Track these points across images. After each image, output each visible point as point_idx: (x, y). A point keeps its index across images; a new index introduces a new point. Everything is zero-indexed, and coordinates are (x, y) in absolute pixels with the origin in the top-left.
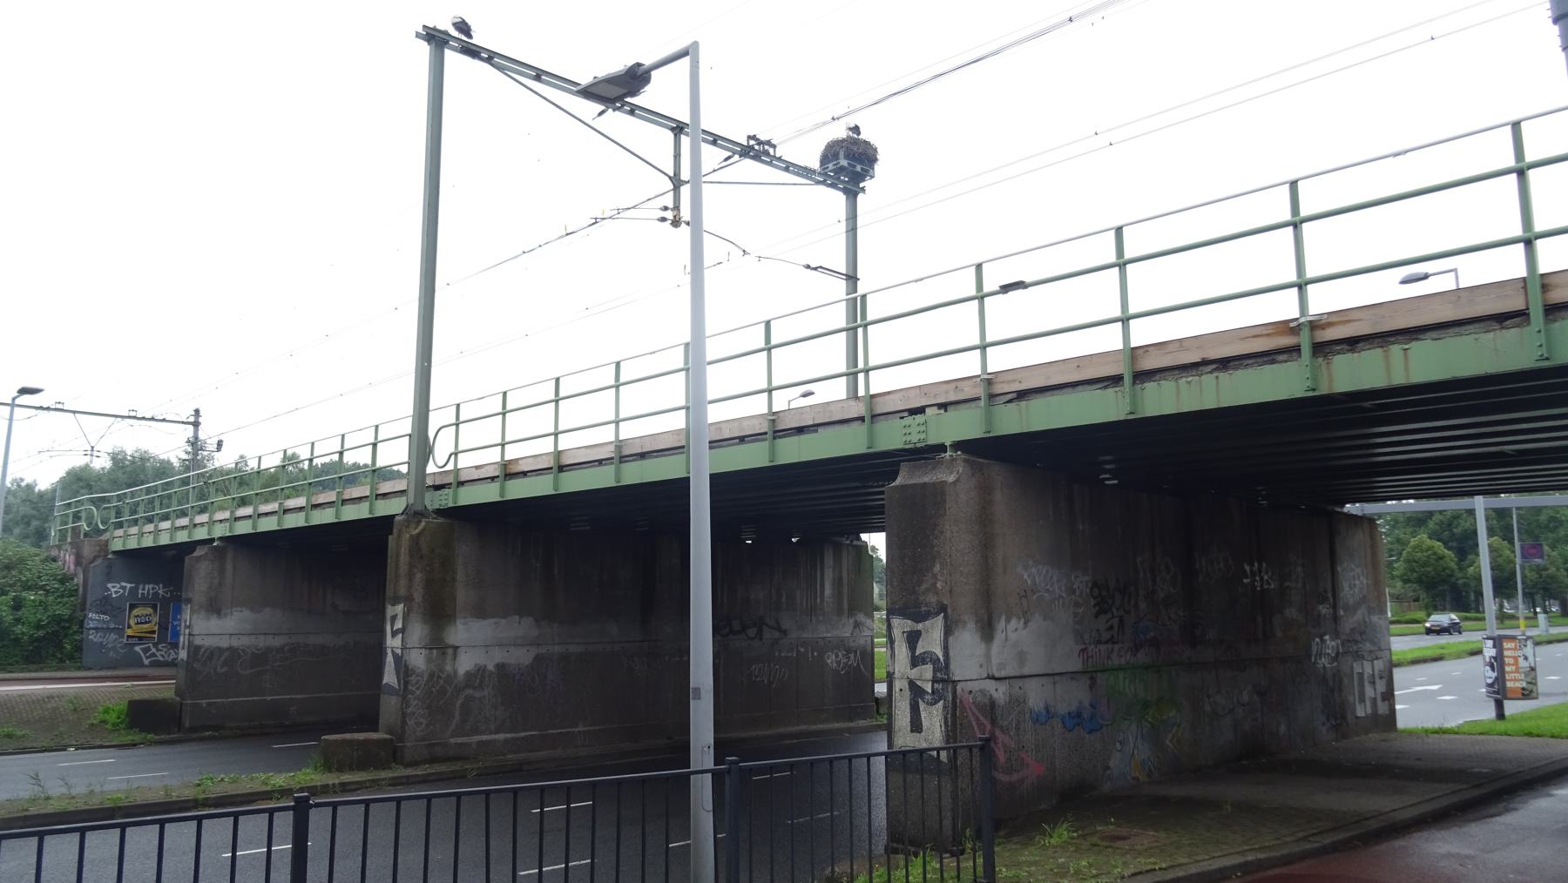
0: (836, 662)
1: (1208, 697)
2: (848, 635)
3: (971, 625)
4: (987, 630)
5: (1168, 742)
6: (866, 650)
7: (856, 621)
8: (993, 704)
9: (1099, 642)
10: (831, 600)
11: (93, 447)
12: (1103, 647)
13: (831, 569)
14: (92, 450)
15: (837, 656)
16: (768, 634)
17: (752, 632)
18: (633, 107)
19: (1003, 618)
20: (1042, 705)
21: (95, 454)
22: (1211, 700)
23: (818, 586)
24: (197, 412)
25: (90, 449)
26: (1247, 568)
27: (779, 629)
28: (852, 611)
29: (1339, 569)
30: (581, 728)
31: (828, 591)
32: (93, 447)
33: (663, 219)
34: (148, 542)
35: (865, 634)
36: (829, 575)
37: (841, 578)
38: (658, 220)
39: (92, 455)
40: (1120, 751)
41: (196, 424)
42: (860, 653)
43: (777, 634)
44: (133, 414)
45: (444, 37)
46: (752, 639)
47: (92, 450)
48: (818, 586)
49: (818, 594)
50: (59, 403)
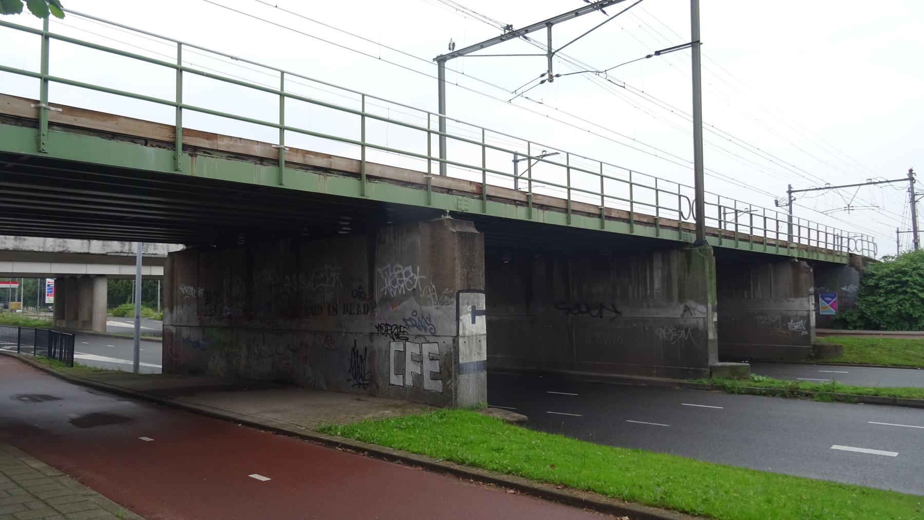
0: (667, 335)
1: (258, 346)
2: (679, 316)
3: (167, 308)
4: (171, 311)
5: (234, 362)
6: (698, 329)
7: (686, 306)
8: (172, 333)
9: (206, 316)
10: (661, 291)
11: (849, 205)
12: (208, 317)
13: (660, 270)
14: (849, 207)
15: (667, 331)
16: (607, 314)
17: (595, 312)
18: (525, 29)
19: (176, 305)
20: (186, 337)
21: (851, 208)
22: (259, 348)
23: (38, 300)
24: (911, 171)
25: (847, 206)
26: (288, 278)
27: (616, 311)
28: (682, 298)
29: (379, 270)
30: (498, 356)
31: (657, 285)
32: (849, 205)
33: (543, 82)
34: (815, 258)
35: (696, 316)
36: (658, 275)
37: (670, 276)
38: (560, 76)
39: (849, 210)
40: (213, 360)
41: (911, 179)
42: (691, 330)
43: (614, 315)
44: (828, 186)
45: (442, 58)
46: (596, 316)
47: (849, 207)
48: (648, 282)
49: (648, 287)
50: (828, 184)
